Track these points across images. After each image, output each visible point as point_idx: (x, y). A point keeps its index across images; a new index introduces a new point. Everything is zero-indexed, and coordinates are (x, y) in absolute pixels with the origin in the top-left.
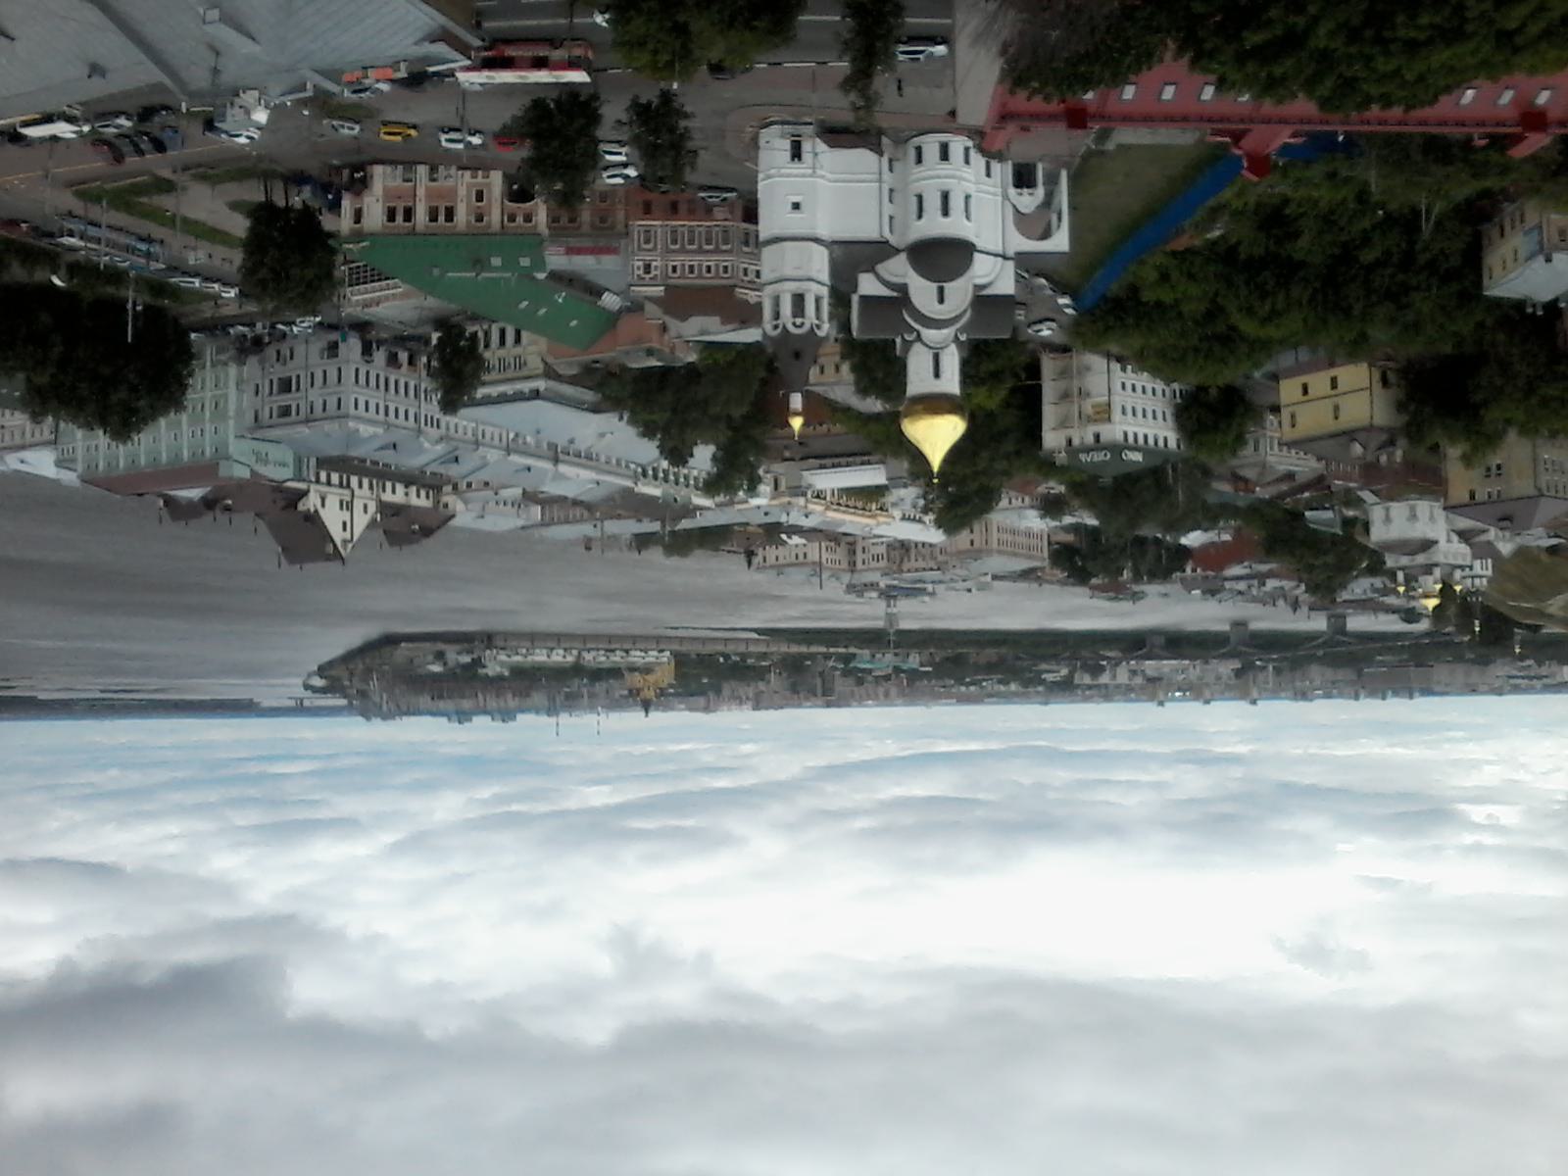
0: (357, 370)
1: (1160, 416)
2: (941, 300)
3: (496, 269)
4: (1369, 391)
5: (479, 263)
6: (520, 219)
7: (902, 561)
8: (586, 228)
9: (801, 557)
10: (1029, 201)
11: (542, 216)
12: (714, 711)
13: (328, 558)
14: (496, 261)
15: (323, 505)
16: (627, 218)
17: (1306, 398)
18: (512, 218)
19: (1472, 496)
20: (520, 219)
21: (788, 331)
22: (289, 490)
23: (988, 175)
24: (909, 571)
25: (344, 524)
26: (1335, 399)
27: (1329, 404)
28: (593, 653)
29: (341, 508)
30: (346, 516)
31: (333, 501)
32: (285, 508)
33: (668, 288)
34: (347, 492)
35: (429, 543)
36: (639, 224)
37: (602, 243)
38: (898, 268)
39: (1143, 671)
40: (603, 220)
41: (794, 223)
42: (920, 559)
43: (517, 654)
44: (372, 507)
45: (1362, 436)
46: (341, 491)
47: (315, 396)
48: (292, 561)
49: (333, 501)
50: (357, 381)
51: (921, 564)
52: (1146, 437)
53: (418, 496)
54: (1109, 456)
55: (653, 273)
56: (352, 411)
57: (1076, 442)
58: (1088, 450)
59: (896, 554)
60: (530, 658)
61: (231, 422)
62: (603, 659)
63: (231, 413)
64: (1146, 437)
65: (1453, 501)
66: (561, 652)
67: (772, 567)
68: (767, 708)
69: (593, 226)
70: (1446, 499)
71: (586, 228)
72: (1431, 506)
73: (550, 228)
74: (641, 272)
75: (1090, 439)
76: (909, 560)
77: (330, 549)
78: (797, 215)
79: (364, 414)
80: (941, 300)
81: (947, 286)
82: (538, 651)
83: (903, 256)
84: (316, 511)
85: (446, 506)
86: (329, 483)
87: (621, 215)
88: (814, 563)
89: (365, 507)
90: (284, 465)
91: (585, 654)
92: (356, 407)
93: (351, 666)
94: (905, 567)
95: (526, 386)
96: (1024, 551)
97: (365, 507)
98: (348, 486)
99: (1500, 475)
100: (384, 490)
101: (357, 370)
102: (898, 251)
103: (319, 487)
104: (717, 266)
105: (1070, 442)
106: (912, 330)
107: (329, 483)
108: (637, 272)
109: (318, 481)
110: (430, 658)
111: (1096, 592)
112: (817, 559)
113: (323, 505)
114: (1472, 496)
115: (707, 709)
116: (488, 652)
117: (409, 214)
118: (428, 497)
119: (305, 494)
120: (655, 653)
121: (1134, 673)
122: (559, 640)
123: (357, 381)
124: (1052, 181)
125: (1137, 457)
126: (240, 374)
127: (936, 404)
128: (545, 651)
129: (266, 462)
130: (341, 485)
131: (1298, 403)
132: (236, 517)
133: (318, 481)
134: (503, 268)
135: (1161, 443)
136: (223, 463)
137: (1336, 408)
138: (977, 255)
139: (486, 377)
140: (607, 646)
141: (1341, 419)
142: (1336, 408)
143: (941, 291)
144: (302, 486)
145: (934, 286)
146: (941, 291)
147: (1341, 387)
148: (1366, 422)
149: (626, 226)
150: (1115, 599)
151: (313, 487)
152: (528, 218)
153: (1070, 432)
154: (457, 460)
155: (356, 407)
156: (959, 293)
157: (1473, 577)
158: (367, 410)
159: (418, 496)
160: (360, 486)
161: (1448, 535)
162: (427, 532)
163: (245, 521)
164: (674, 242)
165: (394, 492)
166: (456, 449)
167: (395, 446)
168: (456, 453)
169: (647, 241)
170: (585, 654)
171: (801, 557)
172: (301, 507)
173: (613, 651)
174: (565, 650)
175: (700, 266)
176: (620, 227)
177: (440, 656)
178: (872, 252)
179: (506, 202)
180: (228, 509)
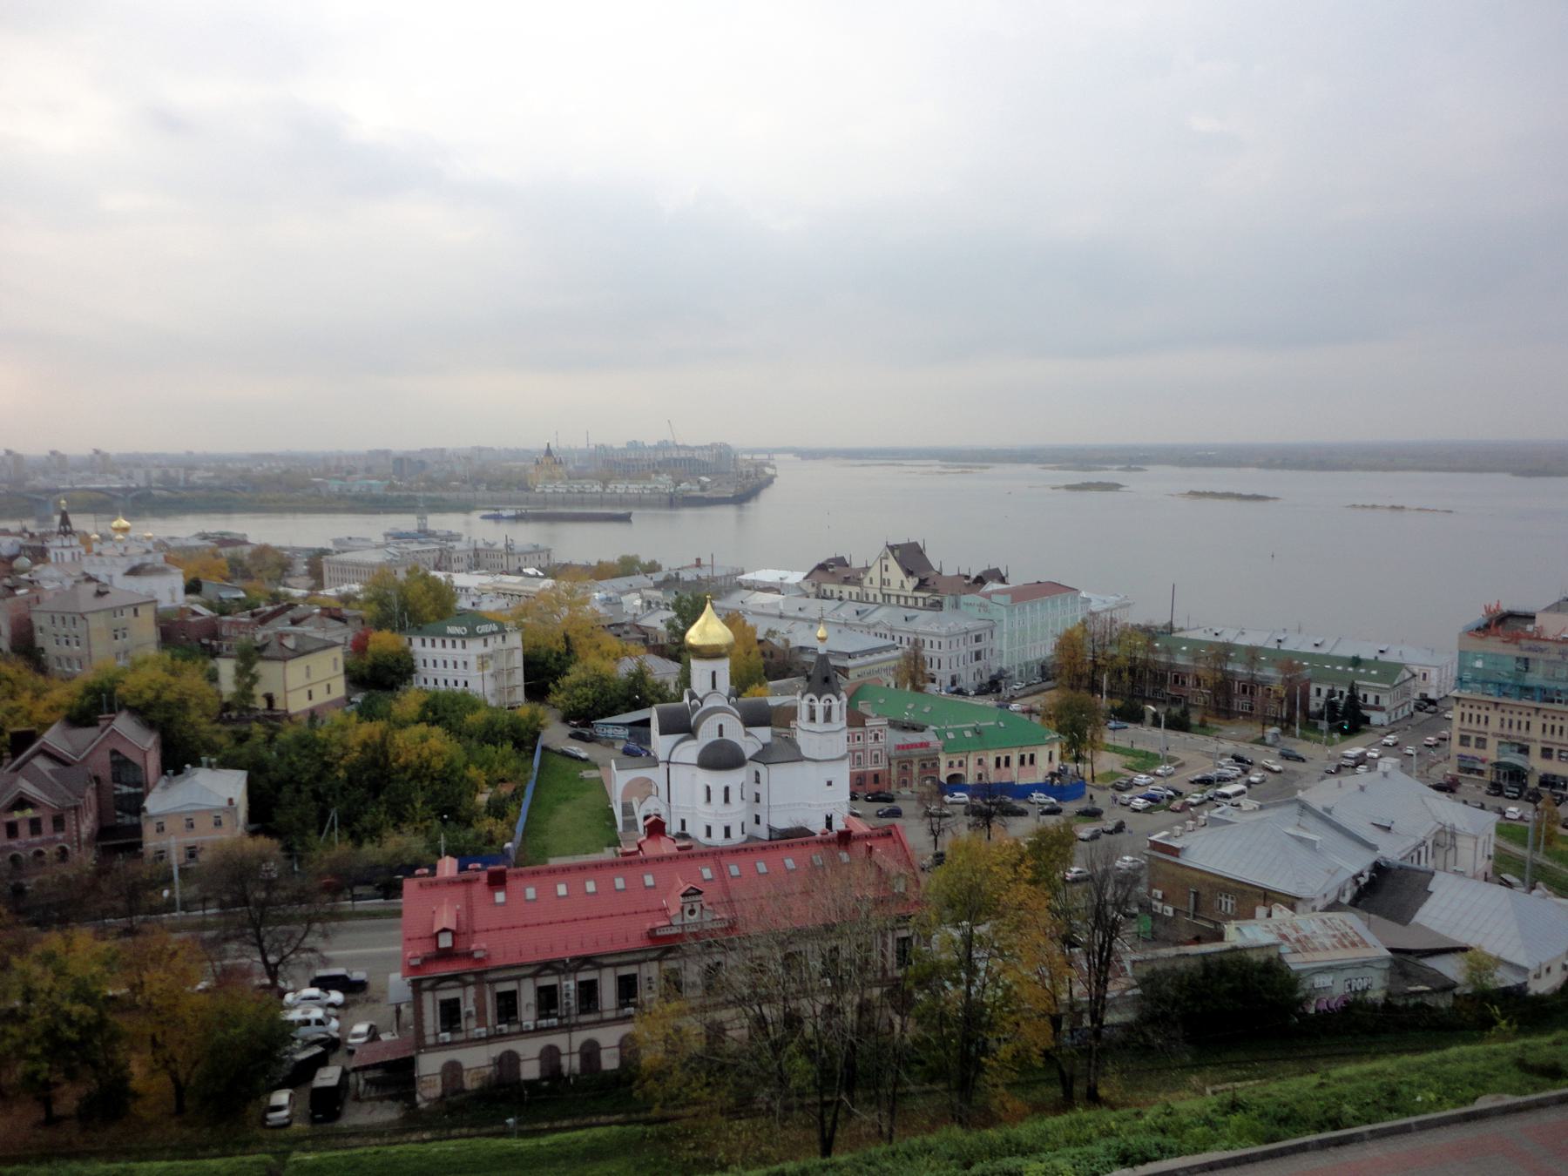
0: (939, 667)
1: (430, 663)
2: (721, 727)
3: (968, 729)
4: (289, 687)
5: (978, 732)
6: (956, 763)
7: (441, 557)
8: (916, 761)
9: (522, 560)
10: (652, 806)
11: (943, 766)
12: (475, 448)
13: (898, 547)
14: (968, 734)
15: (902, 582)
16: (890, 770)
17: (309, 688)
18: (961, 764)
19: (136, 611)
20: (956, 763)
21: (834, 694)
22: (927, 591)
23: (683, 822)
24: (434, 550)
25: (886, 570)
26: (309, 682)
27: (314, 678)
28: (594, 490)
29: (889, 580)
30: (886, 576)
31: (895, 585)
32: (926, 579)
33: (863, 725)
34: (885, 591)
35: (821, 560)
36: (882, 767)
37: (906, 752)
38: (749, 748)
39: (122, 478)
40: (905, 768)
41: (829, 771)
42: (426, 559)
43: (651, 489)
44: (866, 582)
45: (290, 654)
46: (889, 592)
47: (963, 650)
48: (916, 544)
49: (895, 585)
50: (939, 661)
51: (425, 556)
52: (433, 645)
53: (832, 591)
54: (478, 628)
55: (873, 736)
56: (943, 641)
57: (499, 638)
58: (492, 633)
59: (444, 564)
60: (641, 486)
61: (1005, 630)
62: (586, 486)
63: (1005, 636)
64: (433, 645)
65: (151, 607)
66: (618, 491)
67: (542, 551)
68: (435, 450)
69: (911, 763)
70: (156, 611)
71: (916, 761)
72: (174, 601)
73: (938, 759)
74: (880, 734)
75: (490, 640)
76: (434, 558)
77: (897, 553)
78: (829, 778)
79: (933, 639)
80: (721, 727)
81: (717, 738)
82: (636, 492)
83: (748, 755)
84: (907, 577)
85: (813, 585)
86: (898, 596)
87: (894, 771)
88: (513, 554)
89: (871, 582)
90: (967, 604)
91: (600, 490)
92: (940, 643)
93: (756, 481)
94: (437, 554)
95: (859, 661)
96: (362, 569)
97: (871, 582)
98: (884, 595)
99: (115, 631)
100: (857, 594)
101: (939, 667)
102: (751, 759)
103: (906, 594)
104: (854, 741)
105: (504, 638)
106: (733, 704)
107: (898, 596)
108: (883, 734)
109: (906, 598)
110: (709, 487)
111: (241, 539)
112: (510, 558)
113: (902, 582)
114: (136, 611)
115: (480, 450)
116: (672, 490)
117: (1022, 761)
118: (825, 591)
119: (916, 589)
120: (547, 490)
121: (130, 477)
122: (621, 500)
123: (939, 661)
124: (631, 824)
125: (451, 630)
126: (1001, 662)
127: (710, 653)
128: (631, 491)
129: (981, 605)
130: (889, 595)
131: (334, 677)
132: (967, 573)
133: (906, 598)
134: (963, 730)
135: (428, 642)
136: (1009, 603)
137: (308, 675)
138: (695, 762)
139: (893, 663)
140: (585, 496)
141: (305, 666)
142: (308, 675)
143: (721, 734)
144: (917, 594)
145: (726, 736)
146: (721, 734)
147: (305, 693)
148: (290, 663)
149: (890, 764)
150: (222, 534)
151: (910, 594)
152: (951, 764)
153: (504, 647)
154: (858, 613)
155: (940, 643)
156: (707, 734)
157: (71, 546)
158: (932, 642)
159: (832, 591)
160: (875, 596)
161: (111, 581)
162: (822, 567)
163: (949, 571)
164: (859, 758)
165: (850, 593)
166: (860, 620)
167: (906, 619)
168: (859, 617)
169: (876, 756)
170: (600, 490)
171: (522, 560)
172: (917, 580)
173: (580, 492)
174: (615, 492)
175: (854, 741)
176: (894, 763)
177: (703, 489)
178: (765, 756)
179: (964, 773)
180: (967, 577)
